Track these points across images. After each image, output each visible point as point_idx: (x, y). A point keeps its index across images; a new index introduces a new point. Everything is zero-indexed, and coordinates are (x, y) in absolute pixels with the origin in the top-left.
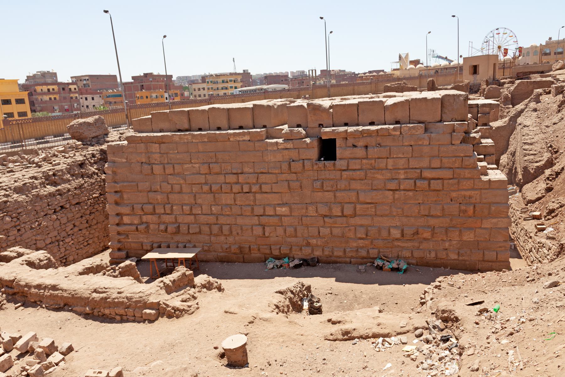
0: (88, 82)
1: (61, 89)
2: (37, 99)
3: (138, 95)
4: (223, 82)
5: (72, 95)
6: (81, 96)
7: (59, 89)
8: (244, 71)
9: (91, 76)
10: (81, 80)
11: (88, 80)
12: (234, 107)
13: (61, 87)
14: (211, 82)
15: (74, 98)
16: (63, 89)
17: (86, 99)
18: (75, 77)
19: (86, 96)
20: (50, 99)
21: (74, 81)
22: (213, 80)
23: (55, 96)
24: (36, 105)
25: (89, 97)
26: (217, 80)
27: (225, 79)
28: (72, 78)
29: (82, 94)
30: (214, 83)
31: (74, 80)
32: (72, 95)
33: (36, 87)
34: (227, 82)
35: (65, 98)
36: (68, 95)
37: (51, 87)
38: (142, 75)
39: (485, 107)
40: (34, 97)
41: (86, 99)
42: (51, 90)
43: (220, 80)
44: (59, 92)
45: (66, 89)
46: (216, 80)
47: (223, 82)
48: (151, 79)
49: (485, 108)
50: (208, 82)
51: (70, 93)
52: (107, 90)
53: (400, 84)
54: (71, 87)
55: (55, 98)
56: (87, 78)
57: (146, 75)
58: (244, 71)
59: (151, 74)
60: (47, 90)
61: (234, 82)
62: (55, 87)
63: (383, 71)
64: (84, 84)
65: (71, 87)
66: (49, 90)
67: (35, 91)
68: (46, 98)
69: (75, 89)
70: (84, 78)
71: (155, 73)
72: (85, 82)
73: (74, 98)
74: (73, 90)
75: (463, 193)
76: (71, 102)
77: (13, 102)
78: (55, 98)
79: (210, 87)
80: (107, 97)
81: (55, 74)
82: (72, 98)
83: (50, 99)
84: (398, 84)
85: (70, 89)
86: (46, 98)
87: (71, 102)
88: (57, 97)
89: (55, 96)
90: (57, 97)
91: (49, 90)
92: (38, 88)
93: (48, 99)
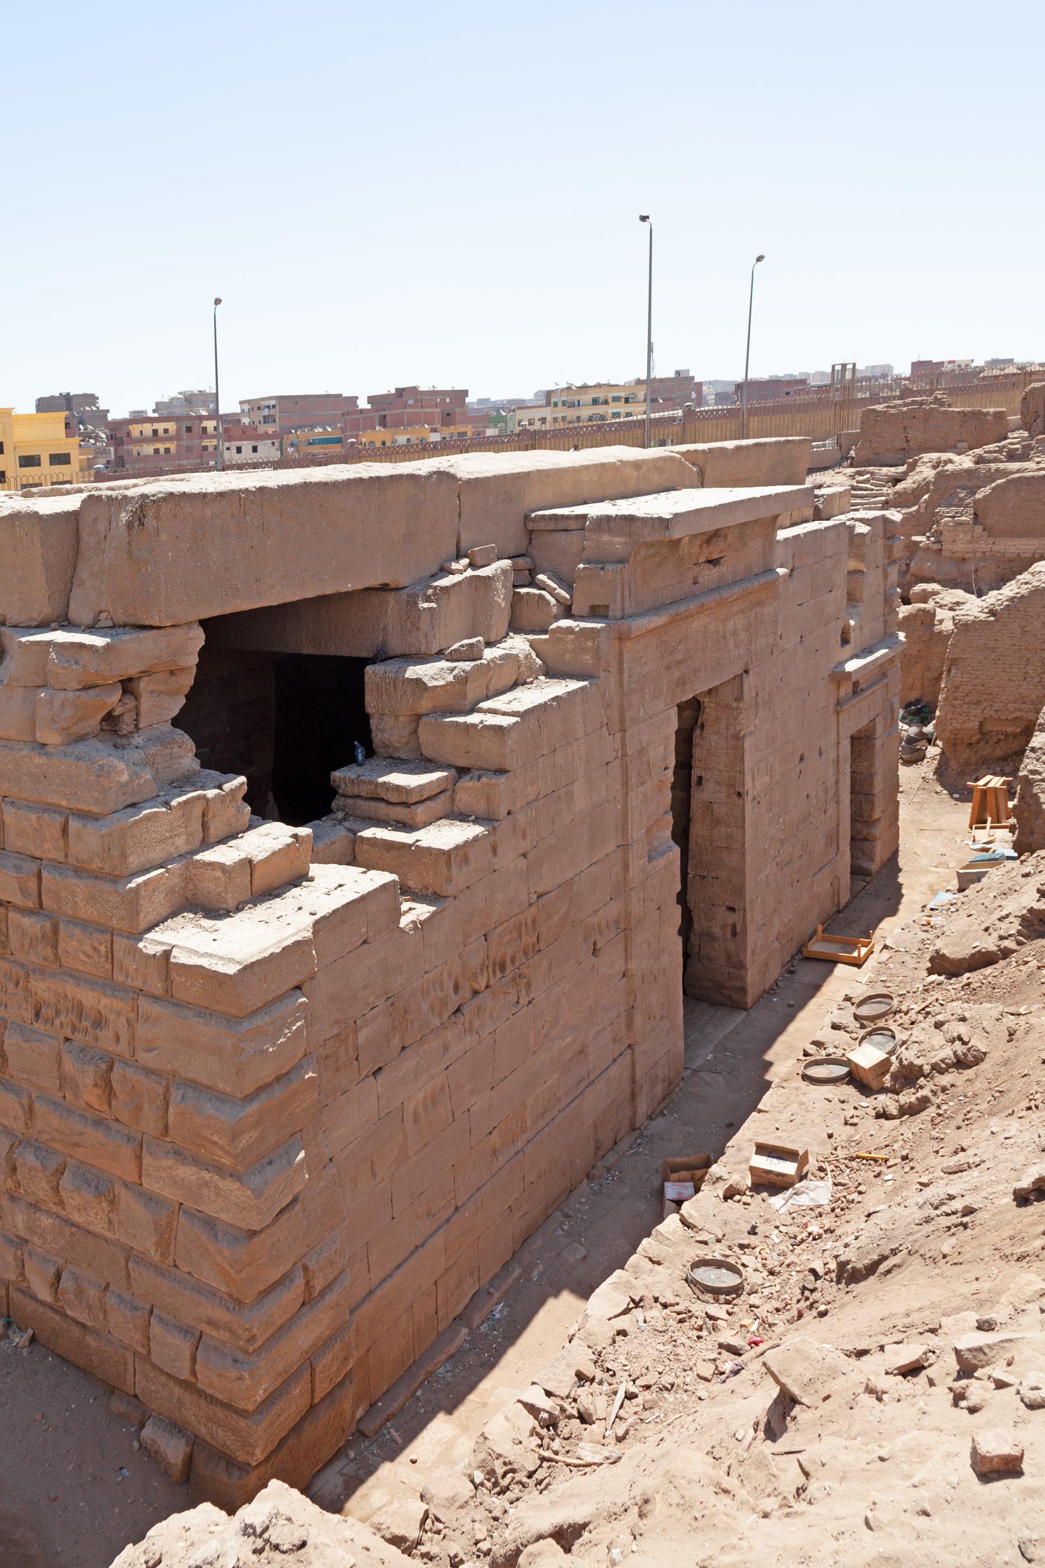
0: (272, 412)
1: (184, 430)
2: (130, 452)
3: (364, 440)
4: (595, 402)
5: (206, 442)
6: (227, 444)
7: (179, 430)
8: (678, 373)
9: (281, 399)
10: (259, 408)
11: (274, 406)
12: (314, 480)
13: (185, 424)
14: (564, 403)
15: (211, 449)
16: (189, 429)
17: (239, 450)
18: (249, 402)
19: (238, 443)
20: (157, 451)
21: (246, 410)
22: (570, 398)
23: (167, 445)
24: (127, 466)
25: (247, 446)
26: (578, 398)
27: (601, 395)
28: (241, 403)
29: (230, 439)
30: (572, 405)
31: (246, 407)
32: (206, 442)
33: (130, 427)
34: (606, 402)
35: (189, 449)
36: (198, 441)
37: (160, 427)
38: (393, 391)
39: (609, 530)
40: (125, 447)
41: (239, 450)
42: (161, 433)
43: (587, 398)
44: (177, 437)
45: (196, 430)
46: (576, 398)
47: (595, 402)
48: (411, 402)
49: (606, 538)
50: (556, 404)
51: (201, 438)
52: (312, 428)
53: (921, 403)
54: (205, 424)
55: (167, 450)
56: (273, 402)
57: (400, 392)
58: (678, 373)
59: (414, 390)
60: (151, 433)
61: (627, 400)
62: (172, 426)
63: (1010, 361)
64: (264, 417)
65: (205, 424)
66: (155, 432)
67: (129, 434)
68: (148, 449)
69: (215, 429)
70: (267, 403)
71: (424, 387)
72: (266, 412)
73: (211, 449)
74: (210, 430)
75: (70, 988)
76: (201, 458)
77: (45, 460)
78: (167, 450)
79: (560, 415)
80: (310, 444)
81: (97, 398)
82: (205, 448)
83: (157, 451)
84: (914, 403)
85: (205, 429)
86: (148, 449)
87: (201, 458)
88: (173, 446)
89: (167, 445)
90: (173, 446)
91: (155, 432)
92: (135, 430)
93: (152, 452)
